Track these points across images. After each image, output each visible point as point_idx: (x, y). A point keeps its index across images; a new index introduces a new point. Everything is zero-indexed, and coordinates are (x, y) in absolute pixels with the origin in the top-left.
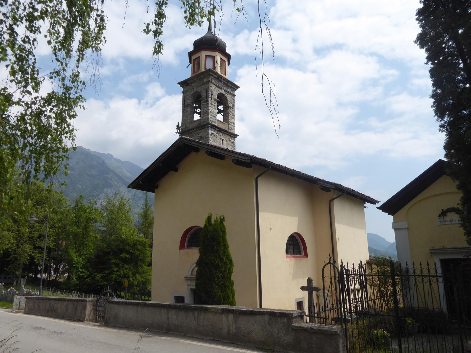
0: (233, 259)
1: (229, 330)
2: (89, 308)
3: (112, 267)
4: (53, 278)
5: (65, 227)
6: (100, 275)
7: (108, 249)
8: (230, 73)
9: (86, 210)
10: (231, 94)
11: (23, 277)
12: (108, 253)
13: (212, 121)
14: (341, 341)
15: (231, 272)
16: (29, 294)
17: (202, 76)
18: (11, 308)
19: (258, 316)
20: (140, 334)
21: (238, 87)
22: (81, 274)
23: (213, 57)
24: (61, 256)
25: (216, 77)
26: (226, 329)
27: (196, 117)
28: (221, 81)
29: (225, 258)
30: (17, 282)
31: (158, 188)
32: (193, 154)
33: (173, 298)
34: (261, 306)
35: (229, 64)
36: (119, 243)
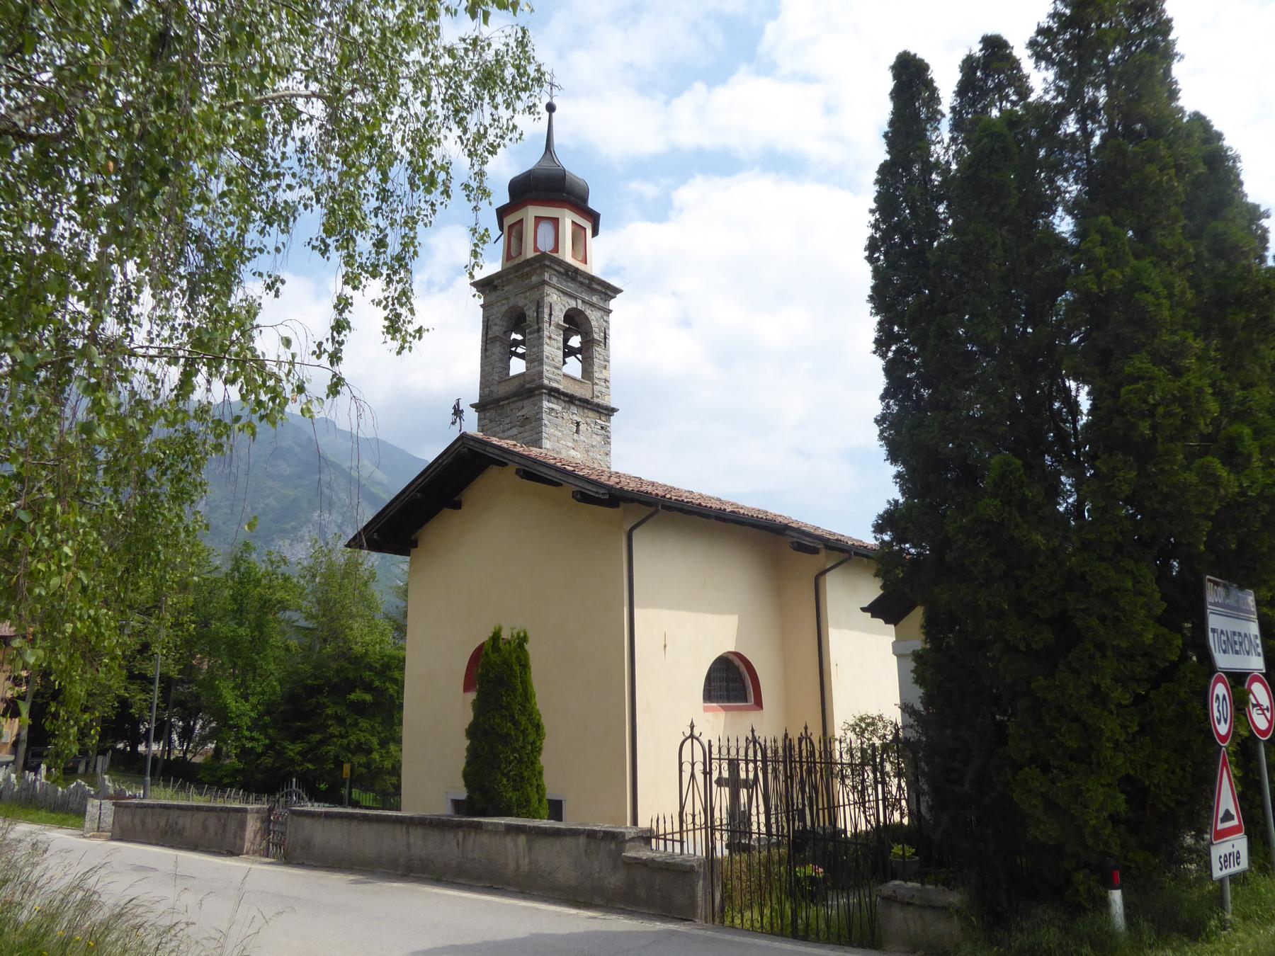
0: (545, 721)
1: (518, 867)
2: (252, 825)
3: (328, 726)
4: (177, 753)
5: (205, 623)
6: (298, 747)
7: (317, 678)
8: (600, 257)
9: (259, 580)
10: (601, 309)
11: (102, 752)
12: (316, 690)
13: (550, 379)
14: (701, 883)
15: (537, 750)
16: (119, 795)
17: (526, 270)
18: (81, 827)
19: (568, 839)
20: (351, 877)
21: (617, 291)
22: (249, 745)
23: (555, 222)
24: (197, 697)
25: (562, 270)
26: (512, 865)
27: (517, 366)
28: (574, 279)
29: (523, 720)
30: (87, 764)
31: (416, 546)
32: (495, 469)
33: (450, 804)
34: (635, 822)
35: (595, 233)
36: (345, 664)
